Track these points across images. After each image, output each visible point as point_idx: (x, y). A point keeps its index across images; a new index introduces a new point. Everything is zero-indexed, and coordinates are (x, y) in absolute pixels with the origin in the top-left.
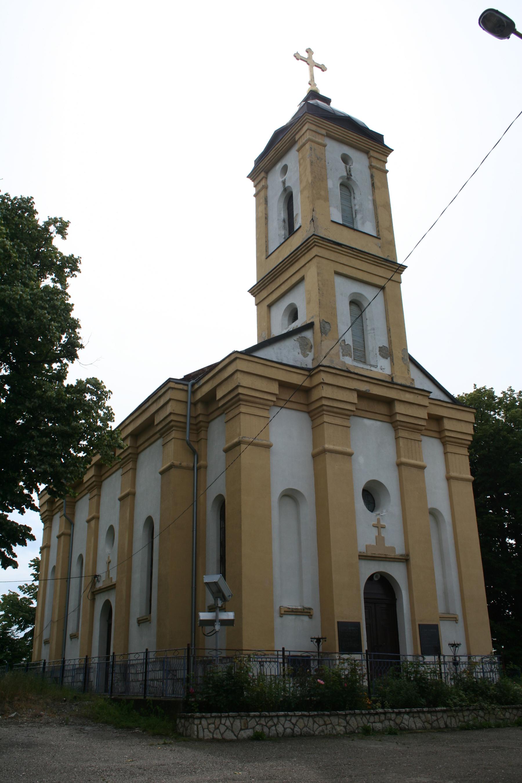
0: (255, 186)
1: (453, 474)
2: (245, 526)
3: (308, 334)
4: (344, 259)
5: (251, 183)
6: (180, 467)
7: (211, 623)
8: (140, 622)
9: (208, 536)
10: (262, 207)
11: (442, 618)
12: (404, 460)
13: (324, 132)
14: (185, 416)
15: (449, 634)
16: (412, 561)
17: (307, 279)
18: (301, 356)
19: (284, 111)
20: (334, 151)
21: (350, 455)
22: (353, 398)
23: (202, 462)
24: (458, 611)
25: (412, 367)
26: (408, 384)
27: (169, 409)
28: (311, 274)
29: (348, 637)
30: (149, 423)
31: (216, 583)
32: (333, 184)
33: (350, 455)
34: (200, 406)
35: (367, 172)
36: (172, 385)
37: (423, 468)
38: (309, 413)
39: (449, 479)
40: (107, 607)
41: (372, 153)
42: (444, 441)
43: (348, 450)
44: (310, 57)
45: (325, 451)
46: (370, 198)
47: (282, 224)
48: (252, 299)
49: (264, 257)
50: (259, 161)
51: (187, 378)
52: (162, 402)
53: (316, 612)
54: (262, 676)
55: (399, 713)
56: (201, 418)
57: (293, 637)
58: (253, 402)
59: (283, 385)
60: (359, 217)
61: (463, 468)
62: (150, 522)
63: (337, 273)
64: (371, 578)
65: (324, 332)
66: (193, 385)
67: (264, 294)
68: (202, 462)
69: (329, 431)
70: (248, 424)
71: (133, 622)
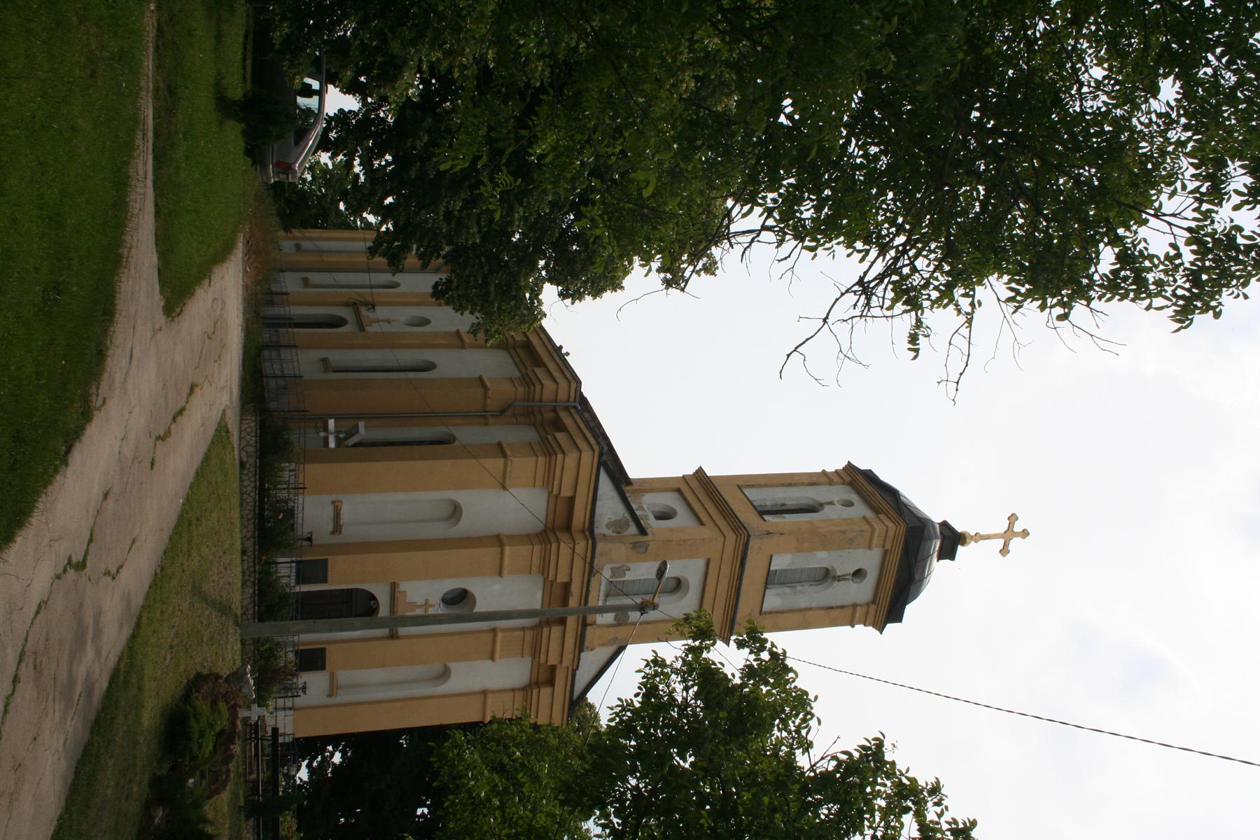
0: (836, 471)
1: (490, 698)
2: (419, 464)
3: (633, 529)
4: (726, 570)
5: (840, 466)
6: (485, 397)
7: (326, 429)
8: (324, 361)
9: (414, 428)
10: (806, 480)
11: (332, 676)
12: (500, 635)
13: (888, 546)
14: (541, 401)
15: (315, 682)
16: (391, 642)
17: (702, 528)
18: (606, 521)
19: (932, 504)
20: (870, 560)
21: (500, 574)
22: (563, 578)
23: (491, 420)
24: (341, 698)
25: (610, 650)
26: (587, 644)
27: (548, 384)
28: (707, 532)
29: (313, 570)
30: (538, 362)
31: (357, 432)
32: (822, 559)
33: (500, 574)
34: (552, 415)
35: (847, 601)
36: (574, 385)
37: (492, 658)
38: (545, 530)
39: (484, 693)
40: (338, 322)
41: (873, 608)
42: (527, 689)
43: (505, 572)
44: (1016, 534)
45: (502, 545)
46: (814, 605)
47: (780, 502)
48: (690, 471)
49: (741, 483)
50: (869, 476)
51: (584, 401)
52: (557, 375)
53: (337, 539)
54: (283, 470)
55: (254, 583)
56: (539, 417)
57: (313, 513)
58: (550, 470)
59: (571, 501)
60: (787, 590)
61: (499, 709)
62: (430, 367)
63: (709, 561)
64: (373, 598)
65: (635, 546)
66: (575, 407)
67: (695, 484)
68: (491, 420)
69: (524, 550)
70: (525, 466)
71: (324, 354)
